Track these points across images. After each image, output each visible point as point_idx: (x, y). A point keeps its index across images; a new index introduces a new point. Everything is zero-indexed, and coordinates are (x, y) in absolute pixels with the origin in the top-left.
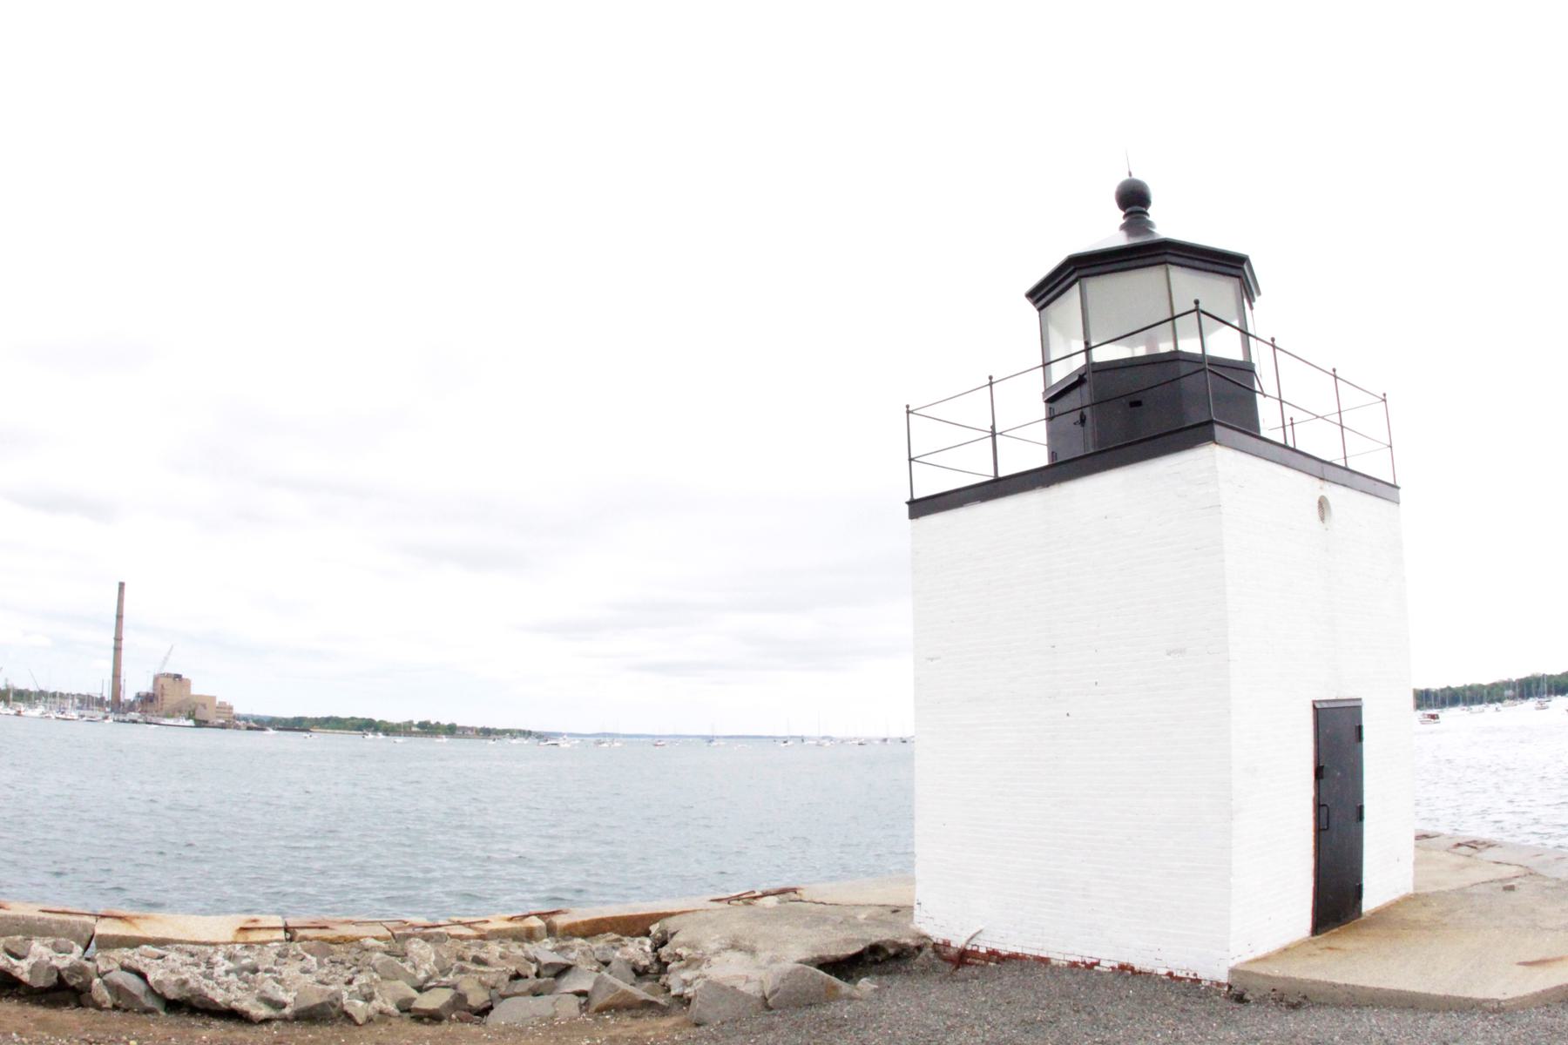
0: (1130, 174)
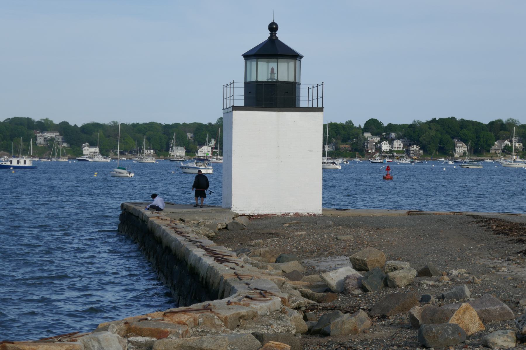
0: (273, 20)
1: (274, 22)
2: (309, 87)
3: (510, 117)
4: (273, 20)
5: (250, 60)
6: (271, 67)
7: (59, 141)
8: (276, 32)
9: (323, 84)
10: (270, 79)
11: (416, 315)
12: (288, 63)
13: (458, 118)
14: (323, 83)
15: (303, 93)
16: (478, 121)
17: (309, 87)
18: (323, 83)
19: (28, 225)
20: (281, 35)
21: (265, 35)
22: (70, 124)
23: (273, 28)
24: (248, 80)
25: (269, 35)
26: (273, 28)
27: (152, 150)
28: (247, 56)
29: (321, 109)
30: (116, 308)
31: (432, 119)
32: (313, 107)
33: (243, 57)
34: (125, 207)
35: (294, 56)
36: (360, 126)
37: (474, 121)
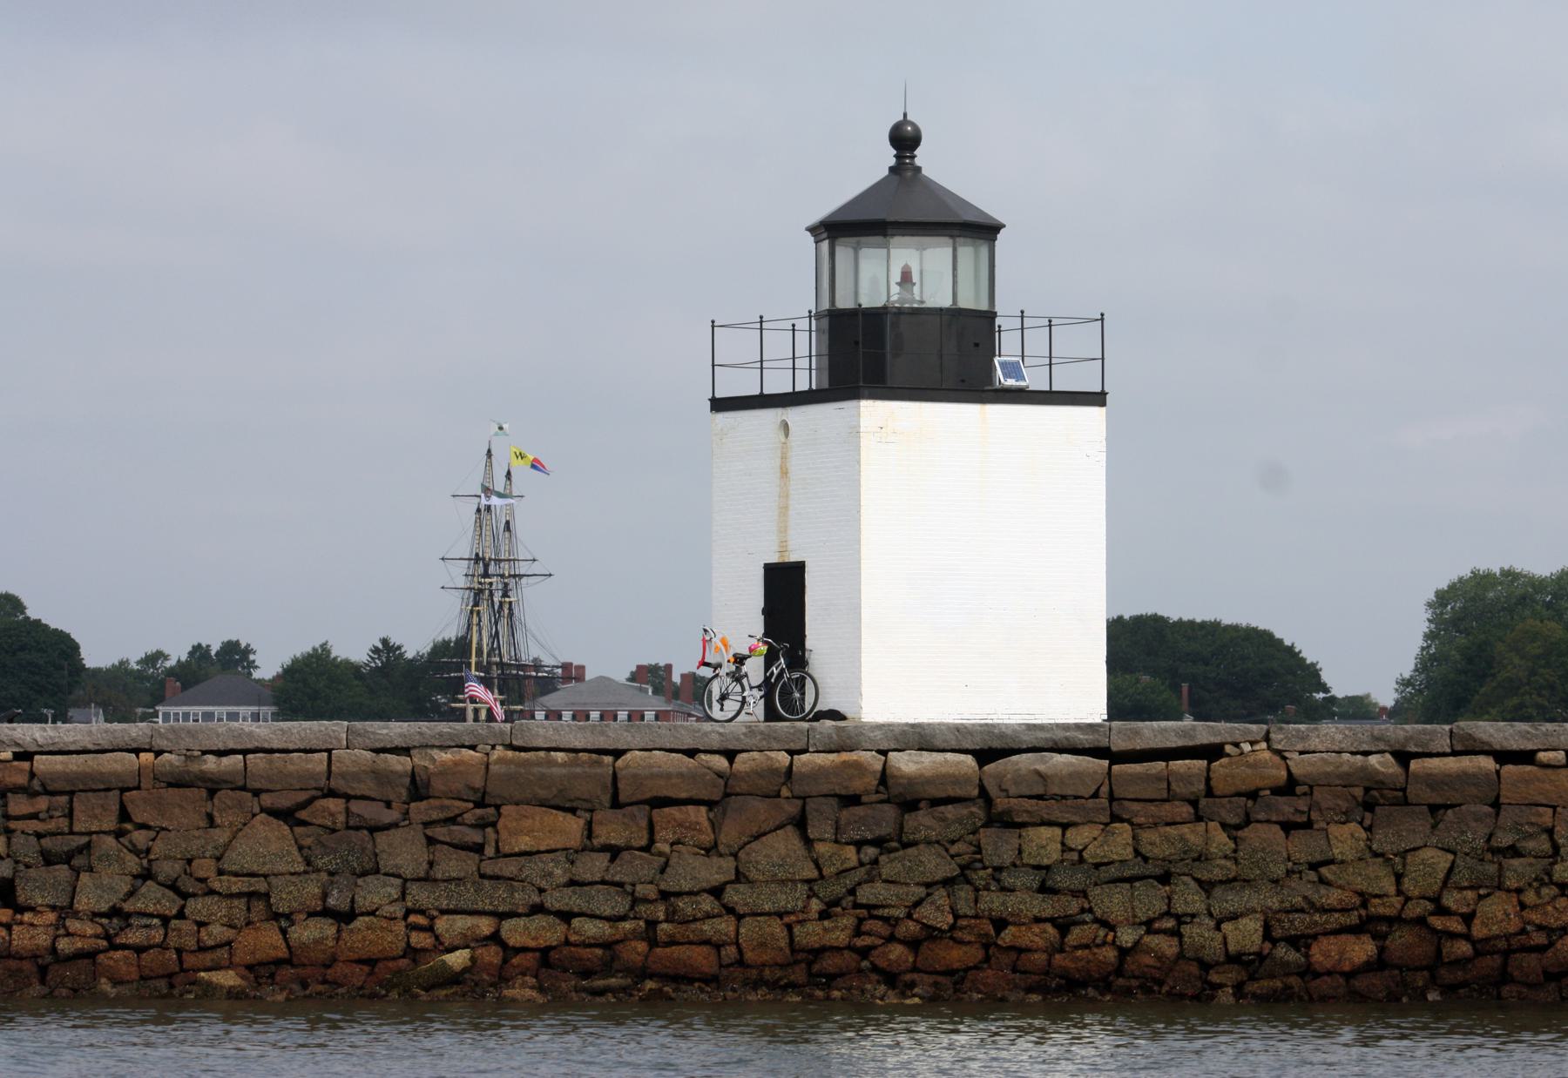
0: (905, 115)
2: (761, 317)
4: (905, 115)
5: (853, 240)
6: (902, 264)
8: (915, 153)
9: (1102, 320)
13: (1198, 620)
14: (1102, 315)
15: (1008, 347)
17: (761, 317)
18: (1102, 315)
23: (905, 140)
24: (844, 302)
25: (892, 161)
26: (905, 140)
29: (1097, 399)
30: (703, 852)
32: (1053, 389)
33: (808, 233)
35: (985, 231)
36: (208, 646)
37: (1426, 663)
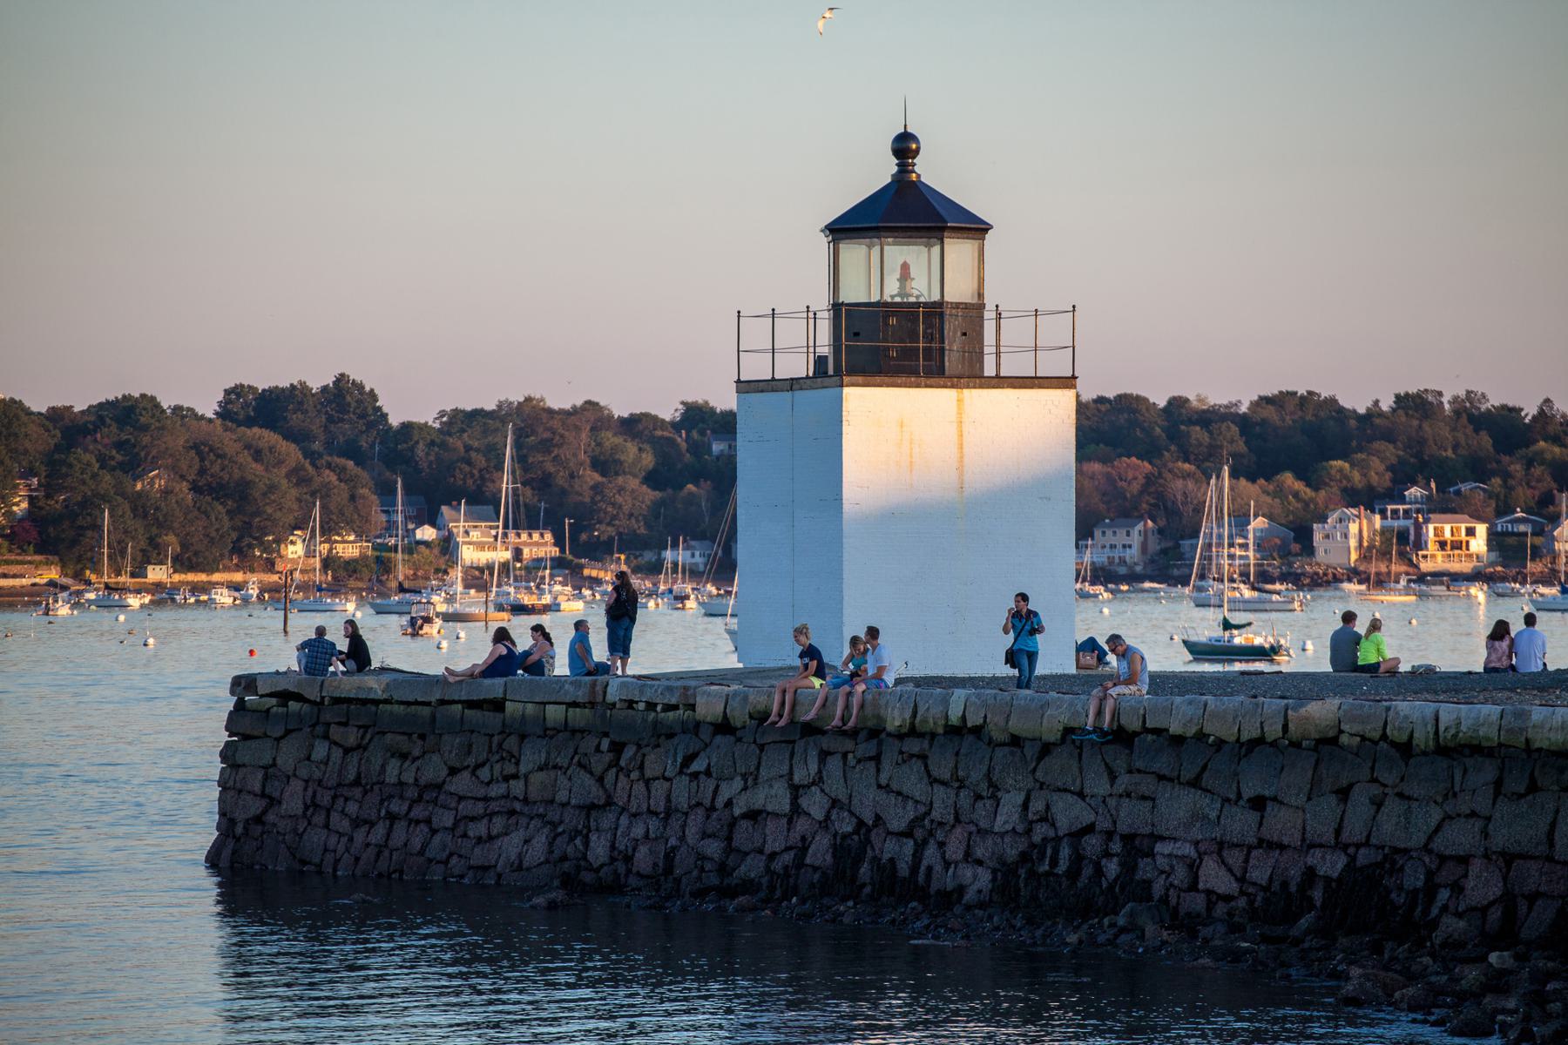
1: (909, 130)
3: (706, 398)
7: (262, 591)
9: (1074, 310)
10: (898, 295)
11: (815, 854)
12: (870, 247)
14: (1074, 307)
16: (653, 413)
18: (1074, 307)
19: (435, 930)
20: (927, 170)
21: (888, 168)
22: (1346, 402)
23: (905, 147)
26: (905, 147)
27: (620, 552)
28: (842, 230)
31: (423, 421)
34: (755, 716)
